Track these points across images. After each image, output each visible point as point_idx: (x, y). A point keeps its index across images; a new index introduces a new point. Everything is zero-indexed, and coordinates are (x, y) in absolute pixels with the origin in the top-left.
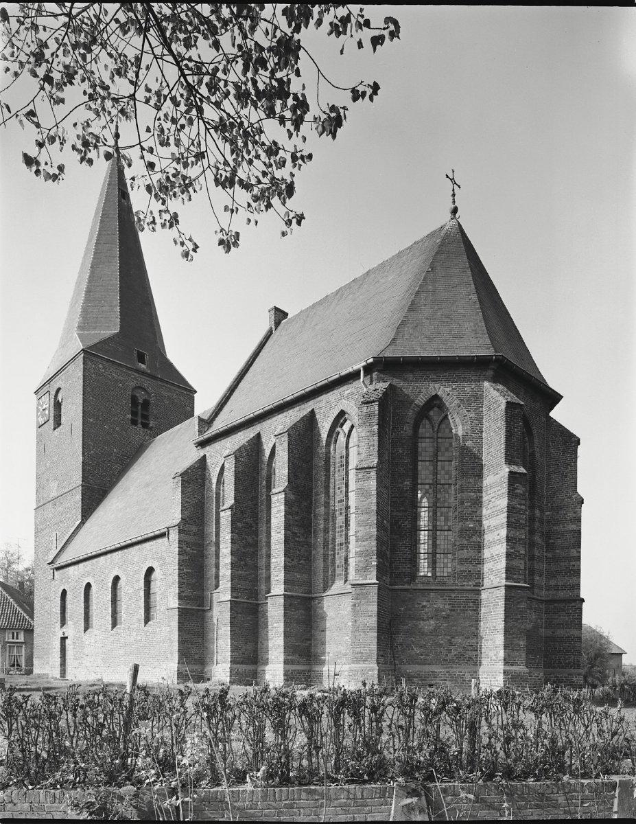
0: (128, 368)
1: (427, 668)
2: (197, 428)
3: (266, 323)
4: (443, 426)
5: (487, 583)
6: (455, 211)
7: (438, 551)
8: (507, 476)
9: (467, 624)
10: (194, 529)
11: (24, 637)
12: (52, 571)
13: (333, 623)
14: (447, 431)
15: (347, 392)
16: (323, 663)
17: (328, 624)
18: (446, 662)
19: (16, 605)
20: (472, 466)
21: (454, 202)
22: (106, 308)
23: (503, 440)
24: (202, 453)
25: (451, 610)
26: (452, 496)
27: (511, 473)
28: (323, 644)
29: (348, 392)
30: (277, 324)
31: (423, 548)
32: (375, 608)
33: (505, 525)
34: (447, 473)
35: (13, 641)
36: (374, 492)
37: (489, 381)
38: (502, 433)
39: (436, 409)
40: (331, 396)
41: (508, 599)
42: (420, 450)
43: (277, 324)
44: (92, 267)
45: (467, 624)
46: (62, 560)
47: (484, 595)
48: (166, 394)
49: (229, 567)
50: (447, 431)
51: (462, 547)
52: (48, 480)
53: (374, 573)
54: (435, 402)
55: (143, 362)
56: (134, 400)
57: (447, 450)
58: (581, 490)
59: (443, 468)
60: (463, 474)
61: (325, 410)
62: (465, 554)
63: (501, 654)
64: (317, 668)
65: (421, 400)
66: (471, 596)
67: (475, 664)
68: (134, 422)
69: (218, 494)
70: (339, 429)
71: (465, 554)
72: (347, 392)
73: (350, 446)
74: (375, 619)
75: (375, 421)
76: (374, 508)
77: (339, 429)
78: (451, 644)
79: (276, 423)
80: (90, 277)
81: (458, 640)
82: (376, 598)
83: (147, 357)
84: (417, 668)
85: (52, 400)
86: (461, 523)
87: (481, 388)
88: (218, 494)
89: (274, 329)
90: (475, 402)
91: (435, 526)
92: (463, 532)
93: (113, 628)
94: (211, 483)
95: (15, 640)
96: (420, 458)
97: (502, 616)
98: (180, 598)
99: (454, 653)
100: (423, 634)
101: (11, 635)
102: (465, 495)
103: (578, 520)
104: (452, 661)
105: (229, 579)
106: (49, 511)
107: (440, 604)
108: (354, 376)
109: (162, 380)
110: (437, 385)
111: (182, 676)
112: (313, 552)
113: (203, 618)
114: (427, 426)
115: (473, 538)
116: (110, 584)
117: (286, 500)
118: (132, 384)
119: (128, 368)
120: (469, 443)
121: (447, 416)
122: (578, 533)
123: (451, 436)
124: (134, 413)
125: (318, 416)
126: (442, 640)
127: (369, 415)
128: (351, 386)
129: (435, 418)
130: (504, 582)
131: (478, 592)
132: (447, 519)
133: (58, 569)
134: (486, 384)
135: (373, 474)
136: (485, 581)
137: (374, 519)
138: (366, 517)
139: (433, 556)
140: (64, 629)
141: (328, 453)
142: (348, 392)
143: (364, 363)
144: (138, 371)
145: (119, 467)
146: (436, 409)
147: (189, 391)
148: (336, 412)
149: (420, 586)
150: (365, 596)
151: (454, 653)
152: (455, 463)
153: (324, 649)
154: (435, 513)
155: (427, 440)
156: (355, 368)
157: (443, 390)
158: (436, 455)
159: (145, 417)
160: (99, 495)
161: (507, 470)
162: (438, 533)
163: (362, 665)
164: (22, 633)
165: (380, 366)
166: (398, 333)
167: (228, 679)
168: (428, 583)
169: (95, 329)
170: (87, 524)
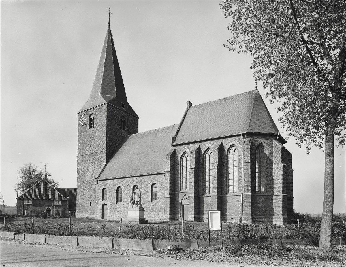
0: (120, 110)
1: (260, 217)
2: (172, 140)
3: (185, 107)
4: (262, 151)
5: (275, 194)
6: (257, 87)
7: (261, 185)
8: (282, 166)
9: (270, 205)
10: (173, 172)
11: (61, 203)
12: (97, 181)
13: (230, 204)
14: (263, 152)
15: (235, 139)
16: (227, 215)
17: (228, 204)
18: (265, 215)
19: (56, 191)
20: (270, 162)
21: (256, 84)
22: (111, 87)
23: (281, 157)
24: (174, 148)
25: (266, 201)
26: (264, 170)
27: (283, 166)
28: (227, 209)
29: (235, 139)
30: (190, 107)
31: (257, 184)
32: (251, 201)
33: (282, 179)
34: (263, 163)
35: (27, 203)
36: (250, 169)
37: (275, 140)
38: (281, 154)
39: (260, 146)
40: (229, 139)
41: (283, 199)
42: (256, 157)
43: (190, 107)
44: (104, 71)
45: (270, 205)
46: (100, 178)
47: (274, 197)
48: (130, 119)
49: (193, 186)
50: (263, 152)
51: (268, 184)
52: (85, 147)
53: (250, 191)
54: (261, 145)
55: (124, 108)
56: (121, 120)
57: (263, 157)
58: (293, 168)
59: (262, 162)
60: (268, 164)
61: (227, 144)
62: (269, 186)
63: (282, 213)
64: (202, 216)
65: (257, 144)
66: (271, 197)
67: (272, 215)
68: (121, 128)
69: (181, 162)
70: (231, 149)
71: (269, 186)
72: (235, 139)
73: (235, 154)
74: (251, 203)
75: (250, 150)
76: (250, 174)
77: (231, 149)
78: (266, 210)
79: (207, 144)
80: (104, 74)
81: (268, 209)
82: (251, 198)
83: (125, 105)
84: (257, 217)
85: (88, 118)
86: (268, 178)
87: (272, 141)
88: (181, 162)
89: (189, 108)
90: (271, 145)
91: (260, 178)
92: (268, 180)
93: (102, 201)
94: (178, 158)
95: (58, 204)
96: (256, 159)
97: (282, 203)
98: (170, 194)
99: (267, 212)
100: (259, 207)
101: (56, 202)
102: (269, 170)
103: (292, 176)
104: (266, 215)
105: (194, 190)
106: (80, 158)
107: (263, 199)
108: (240, 135)
109: (130, 114)
110: (261, 140)
111: (170, 218)
112: (222, 183)
113: (175, 200)
114: (258, 150)
115: (270, 182)
116: (132, 188)
117: (218, 168)
118: (121, 115)
119: (120, 110)
120: (270, 156)
121: (263, 148)
122: (292, 180)
123: (264, 154)
124: (121, 125)
125: (224, 144)
126: (263, 209)
127: (248, 148)
128: (236, 138)
129: (260, 148)
130: (282, 194)
131: (272, 196)
132: (263, 176)
133: (99, 181)
134: (274, 141)
135: (249, 164)
136: (274, 193)
137: (250, 176)
138: (248, 176)
139: (260, 186)
140: (104, 202)
141: (227, 155)
142: (235, 139)
143: (243, 133)
144: (123, 110)
145: (116, 144)
146: (260, 146)
147: (136, 117)
148: (231, 144)
149: (258, 194)
150: (247, 197)
151: (267, 212)
152: (266, 161)
153: (227, 211)
154: (260, 174)
155: (258, 154)
156: (240, 133)
157: (263, 141)
158: (260, 158)
159: (124, 126)
160: (111, 154)
161: (282, 165)
162: (261, 180)
163: (246, 216)
164: (61, 201)
165: (248, 134)
166: (250, 124)
167: (194, 220)
168: (259, 193)
169: (107, 94)
170: (109, 164)
